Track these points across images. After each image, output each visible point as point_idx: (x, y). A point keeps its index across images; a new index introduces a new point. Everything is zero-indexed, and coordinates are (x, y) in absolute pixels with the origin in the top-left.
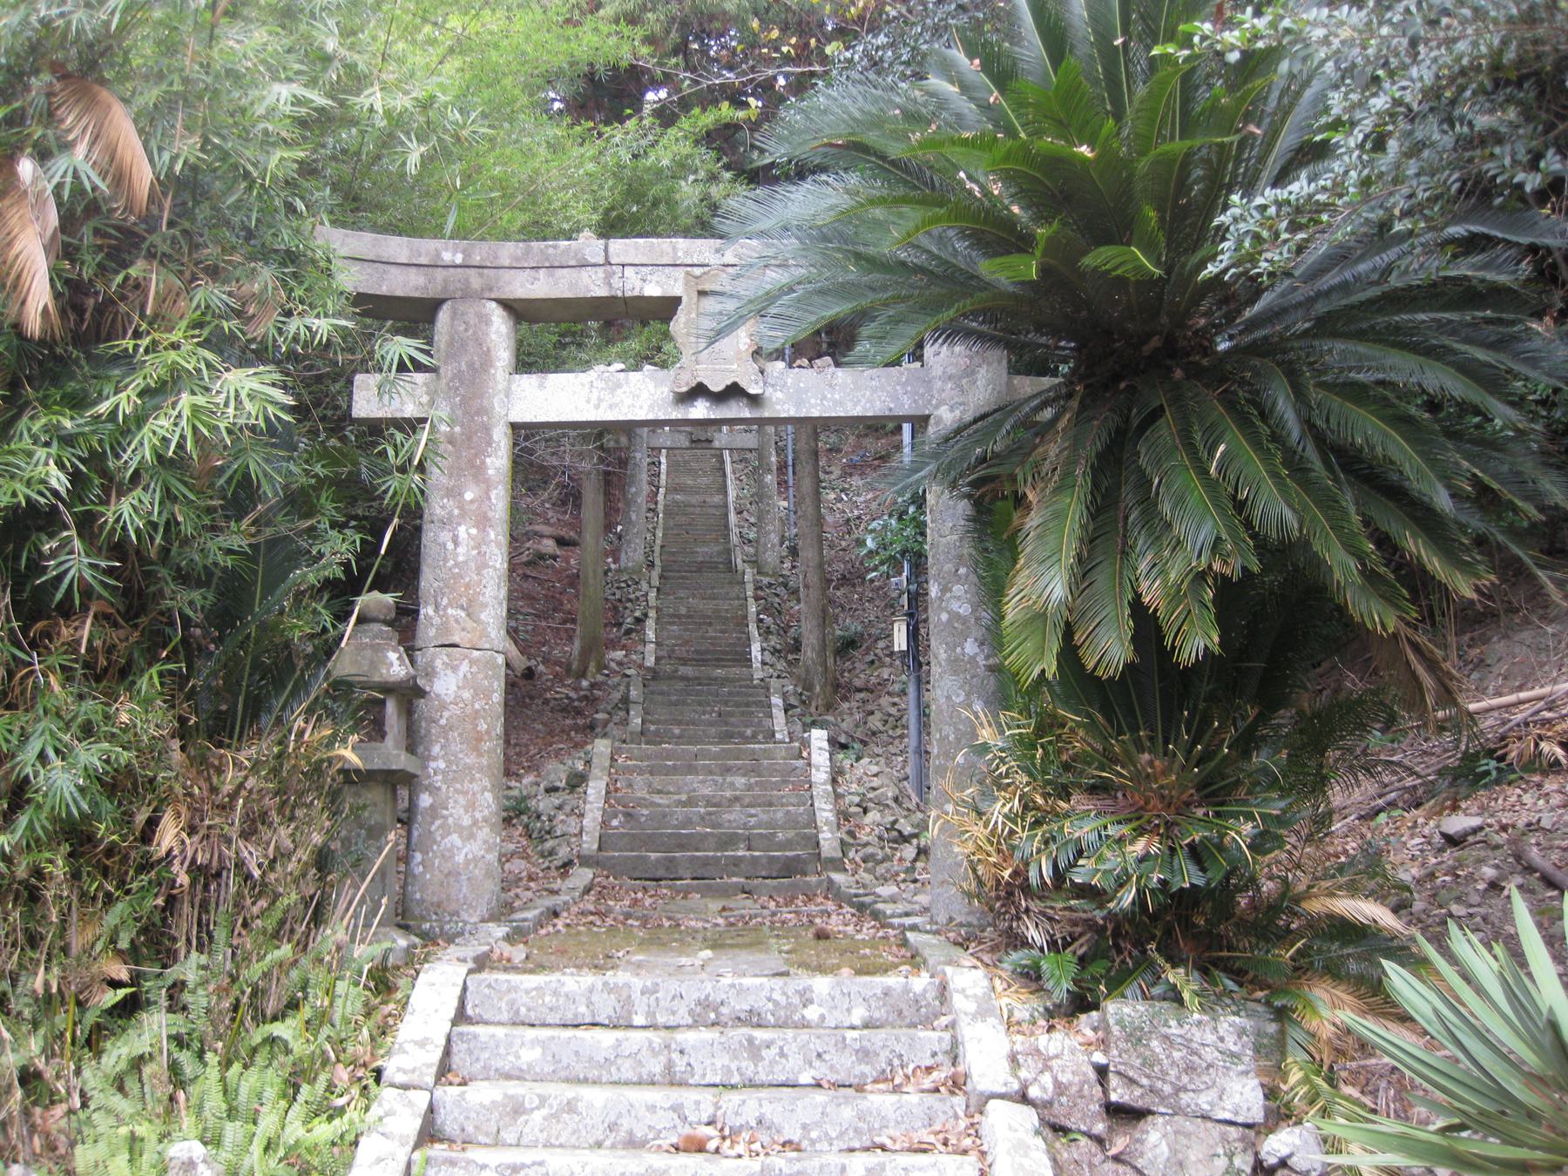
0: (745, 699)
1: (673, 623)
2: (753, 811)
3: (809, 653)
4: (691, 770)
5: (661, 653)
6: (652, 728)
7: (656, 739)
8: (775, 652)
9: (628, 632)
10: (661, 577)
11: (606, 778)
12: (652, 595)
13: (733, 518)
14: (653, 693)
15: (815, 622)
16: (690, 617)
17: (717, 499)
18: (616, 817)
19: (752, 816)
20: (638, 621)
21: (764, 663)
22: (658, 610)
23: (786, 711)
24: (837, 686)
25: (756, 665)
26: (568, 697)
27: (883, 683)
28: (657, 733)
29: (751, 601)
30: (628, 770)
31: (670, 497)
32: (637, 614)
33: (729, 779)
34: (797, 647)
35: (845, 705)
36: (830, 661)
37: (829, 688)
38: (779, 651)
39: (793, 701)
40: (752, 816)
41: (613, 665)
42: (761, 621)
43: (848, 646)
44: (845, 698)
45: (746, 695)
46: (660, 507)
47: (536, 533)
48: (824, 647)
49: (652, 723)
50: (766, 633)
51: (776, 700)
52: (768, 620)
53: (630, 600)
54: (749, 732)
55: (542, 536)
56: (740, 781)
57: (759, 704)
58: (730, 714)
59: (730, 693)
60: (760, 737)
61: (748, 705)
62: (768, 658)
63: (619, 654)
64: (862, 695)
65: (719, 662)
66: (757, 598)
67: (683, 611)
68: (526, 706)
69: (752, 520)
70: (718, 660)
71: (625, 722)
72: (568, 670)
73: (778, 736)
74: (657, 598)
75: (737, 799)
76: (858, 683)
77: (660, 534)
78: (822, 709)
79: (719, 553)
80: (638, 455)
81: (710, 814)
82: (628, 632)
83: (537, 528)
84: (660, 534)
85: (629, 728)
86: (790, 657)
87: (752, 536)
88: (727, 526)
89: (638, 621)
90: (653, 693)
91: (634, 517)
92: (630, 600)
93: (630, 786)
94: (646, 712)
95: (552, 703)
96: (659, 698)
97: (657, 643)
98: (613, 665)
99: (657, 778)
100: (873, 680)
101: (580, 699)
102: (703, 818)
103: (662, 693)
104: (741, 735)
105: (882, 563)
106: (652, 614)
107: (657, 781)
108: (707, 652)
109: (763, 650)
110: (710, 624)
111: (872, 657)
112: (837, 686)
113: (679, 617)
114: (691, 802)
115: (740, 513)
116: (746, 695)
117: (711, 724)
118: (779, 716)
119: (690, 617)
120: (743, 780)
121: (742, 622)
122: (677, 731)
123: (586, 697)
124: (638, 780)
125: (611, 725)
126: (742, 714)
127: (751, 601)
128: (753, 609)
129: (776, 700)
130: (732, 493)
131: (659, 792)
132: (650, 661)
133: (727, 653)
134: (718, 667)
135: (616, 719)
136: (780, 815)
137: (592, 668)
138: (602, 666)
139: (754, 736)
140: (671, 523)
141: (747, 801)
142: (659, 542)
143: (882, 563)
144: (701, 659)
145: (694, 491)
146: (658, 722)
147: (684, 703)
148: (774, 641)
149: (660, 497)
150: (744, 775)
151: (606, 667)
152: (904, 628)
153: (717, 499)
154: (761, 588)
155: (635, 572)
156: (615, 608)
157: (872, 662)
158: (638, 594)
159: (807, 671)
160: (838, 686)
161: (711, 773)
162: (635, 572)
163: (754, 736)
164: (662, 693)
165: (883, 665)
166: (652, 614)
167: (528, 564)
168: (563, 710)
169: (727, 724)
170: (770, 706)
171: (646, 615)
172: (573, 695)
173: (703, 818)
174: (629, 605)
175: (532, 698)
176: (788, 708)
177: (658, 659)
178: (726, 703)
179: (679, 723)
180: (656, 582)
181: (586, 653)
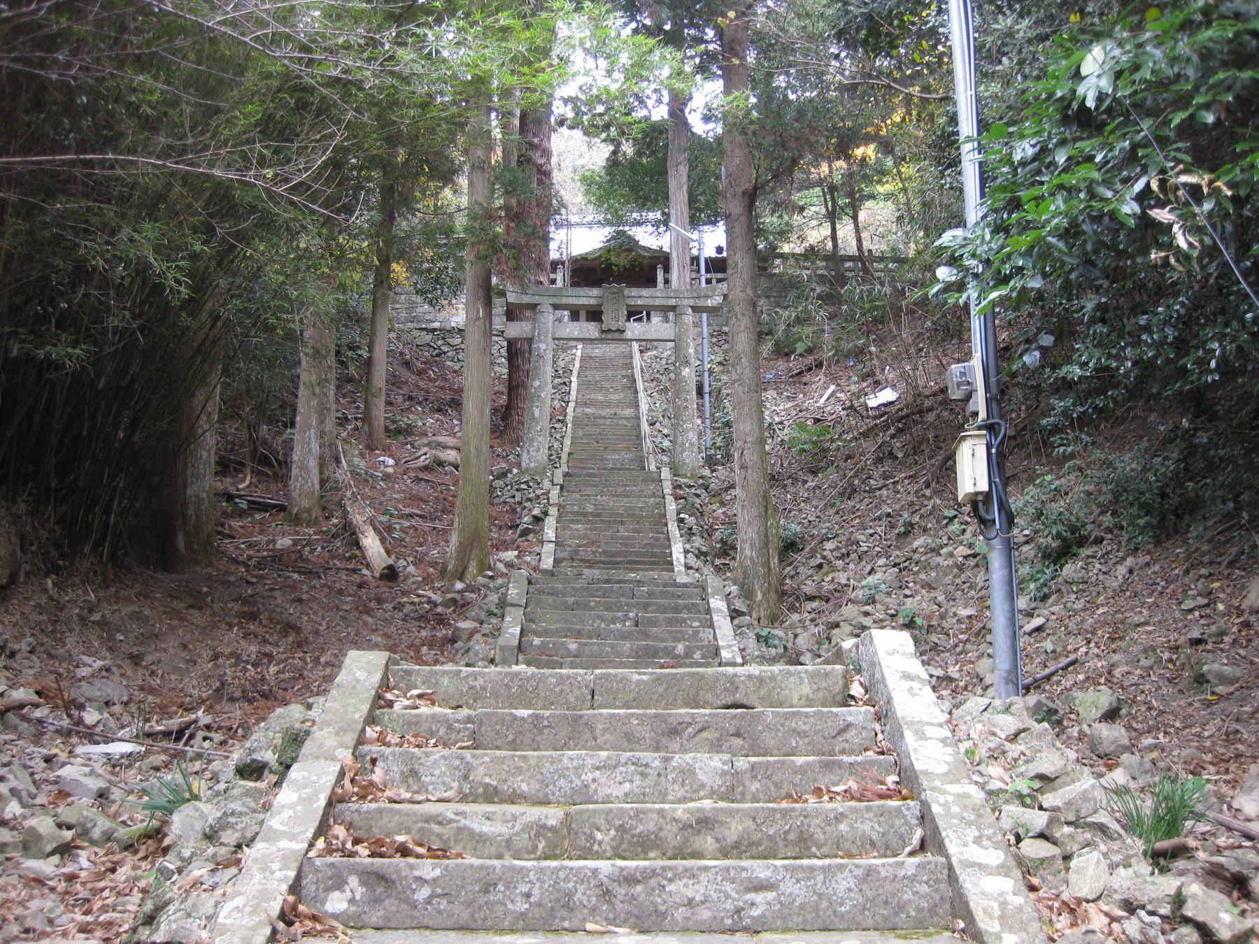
0: (672, 602)
1: (578, 522)
2: (760, 869)
3: (747, 551)
4: (577, 732)
5: (562, 555)
6: (537, 641)
7: (544, 658)
8: (700, 554)
9: (525, 533)
10: (566, 475)
11: (345, 755)
12: (555, 492)
13: (645, 427)
14: (541, 592)
15: (754, 512)
16: (598, 515)
17: (629, 412)
18: (339, 883)
19: (759, 887)
20: (537, 520)
21: (688, 567)
22: (560, 507)
23: (732, 619)
24: (782, 594)
25: (679, 567)
26: (430, 601)
27: (841, 589)
28: (542, 649)
29: (669, 499)
30: (421, 733)
31: (579, 410)
32: (536, 512)
33: (678, 760)
34: (727, 549)
35: (796, 617)
36: (775, 561)
37: (773, 596)
38: (705, 554)
39: (739, 605)
40: (759, 887)
41: (500, 566)
42: (681, 521)
43: (790, 547)
44: (793, 609)
45: (674, 596)
46: (569, 418)
47: (439, 444)
48: (766, 544)
49: (536, 633)
50: (689, 534)
51: (717, 603)
52: (691, 521)
53: (529, 500)
54: (680, 648)
55: (445, 447)
56: (709, 766)
57: (692, 608)
58: (654, 623)
59: (650, 594)
60: (697, 656)
61: (676, 609)
62: (692, 561)
63: (510, 555)
64: (815, 604)
65: (633, 565)
66: (677, 498)
67: (590, 508)
68: (369, 611)
69: (665, 431)
70: (630, 562)
71: (496, 632)
72: (443, 571)
73: (725, 654)
74: (560, 495)
75: (705, 823)
76: (809, 588)
77: (567, 442)
78: (764, 622)
79: (631, 461)
80: (543, 346)
81: (630, 879)
82: (525, 533)
83: (441, 439)
84: (567, 442)
85: (501, 641)
86: (718, 562)
87: (666, 443)
88: (638, 436)
89: (537, 520)
90: (541, 592)
91: (537, 413)
92: (529, 500)
93: (413, 774)
94: (529, 619)
95: (408, 608)
96: (550, 600)
97: (557, 543)
98: (500, 566)
99: (487, 755)
100: (826, 586)
101: (445, 604)
102: (606, 894)
103: (555, 593)
104: (669, 652)
105: (1048, 221)
106: (553, 511)
107: (486, 766)
108: (618, 554)
109: (686, 552)
110: (622, 523)
111: (819, 561)
112: (782, 594)
113: (585, 515)
114: (562, 841)
115: (653, 424)
116: (674, 596)
117: (625, 637)
118: (724, 628)
119: (598, 515)
120: (716, 762)
121: (661, 519)
122: (573, 646)
123: (454, 601)
124: (437, 762)
125: (478, 636)
126: (670, 622)
127: (669, 499)
128: (672, 506)
129: (717, 603)
130: (644, 407)
131: (491, 795)
132: (547, 563)
133: (643, 555)
134: (632, 570)
135: (486, 628)
136: (843, 883)
137: (472, 568)
138: (484, 566)
139: (688, 654)
140: (580, 433)
141: (734, 830)
142: (566, 449)
143: (1048, 221)
144: (610, 561)
145: (607, 404)
146: (546, 633)
147: (586, 606)
148: (698, 542)
149: (570, 410)
150: (716, 747)
151: (490, 568)
152: (982, 451)
153: (629, 412)
154: (680, 487)
155: (537, 473)
156: (513, 511)
157: (820, 566)
158: (539, 492)
159: (745, 572)
160: (784, 593)
161: (630, 740)
162: (537, 473)
163: (688, 654)
164: (555, 593)
165: (834, 569)
166: (553, 511)
167: (425, 468)
168: (419, 618)
169: (647, 636)
170: (708, 611)
171: (546, 514)
172: (436, 598)
173: (606, 894)
174: (528, 504)
175: (380, 601)
176: (734, 614)
177: (557, 562)
178: (645, 607)
179: (578, 634)
180: (559, 479)
181: (465, 549)
